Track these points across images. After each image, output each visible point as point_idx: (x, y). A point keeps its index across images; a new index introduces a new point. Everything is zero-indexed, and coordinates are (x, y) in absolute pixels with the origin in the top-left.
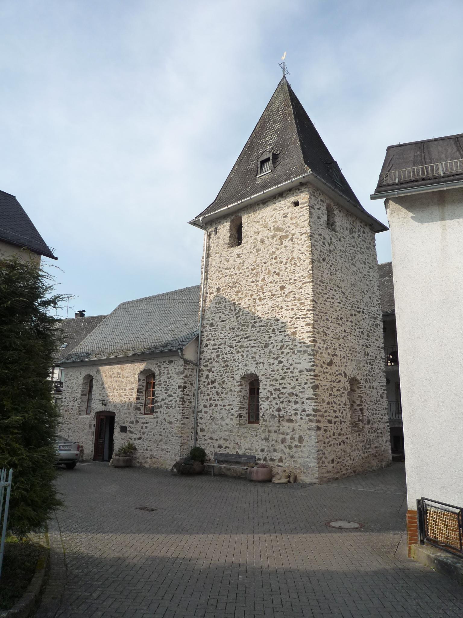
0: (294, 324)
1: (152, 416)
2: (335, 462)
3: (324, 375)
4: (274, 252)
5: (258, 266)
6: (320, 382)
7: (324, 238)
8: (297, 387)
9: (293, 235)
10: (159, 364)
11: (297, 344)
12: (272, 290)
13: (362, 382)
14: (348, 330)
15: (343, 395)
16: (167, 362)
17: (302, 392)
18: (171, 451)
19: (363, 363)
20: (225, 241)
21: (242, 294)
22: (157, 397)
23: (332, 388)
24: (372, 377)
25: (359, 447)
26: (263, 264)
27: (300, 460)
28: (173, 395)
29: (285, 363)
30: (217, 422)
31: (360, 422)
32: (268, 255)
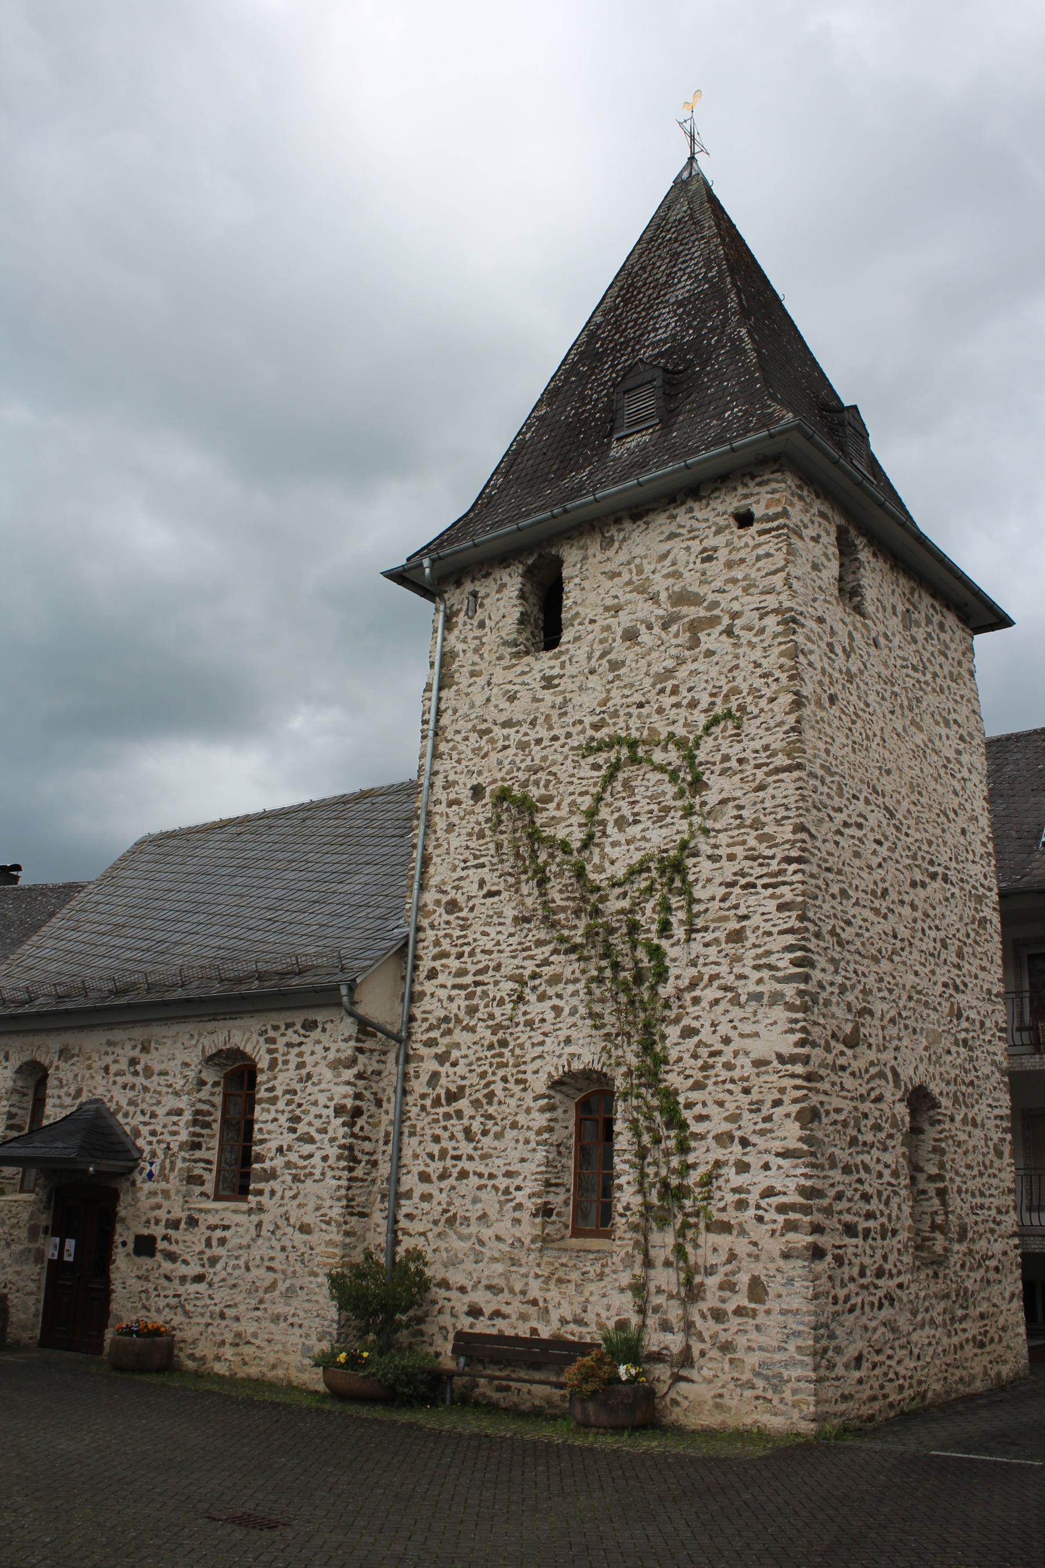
0: (736, 907)
1: (244, 1206)
2: (866, 1365)
3: (834, 1078)
4: (669, 673)
5: (615, 714)
6: (822, 1098)
7: (833, 633)
8: (746, 1115)
9: (735, 616)
10: (271, 1033)
11: (747, 971)
12: (664, 793)
13: (944, 1101)
14: (904, 933)
16: (298, 1027)
17: (762, 1133)
18: (306, 1323)
19: (947, 1042)
20: (503, 634)
21: (558, 807)
22: (262, 1141)
23: (857, 1120)
24: (970, 1090)
25: (935, 1315)
26: (633, 710)
27: (753, 1359)
28: (317, 1137)
29: (705, 1035)
30: (464, 1230)
32: (648, 682)
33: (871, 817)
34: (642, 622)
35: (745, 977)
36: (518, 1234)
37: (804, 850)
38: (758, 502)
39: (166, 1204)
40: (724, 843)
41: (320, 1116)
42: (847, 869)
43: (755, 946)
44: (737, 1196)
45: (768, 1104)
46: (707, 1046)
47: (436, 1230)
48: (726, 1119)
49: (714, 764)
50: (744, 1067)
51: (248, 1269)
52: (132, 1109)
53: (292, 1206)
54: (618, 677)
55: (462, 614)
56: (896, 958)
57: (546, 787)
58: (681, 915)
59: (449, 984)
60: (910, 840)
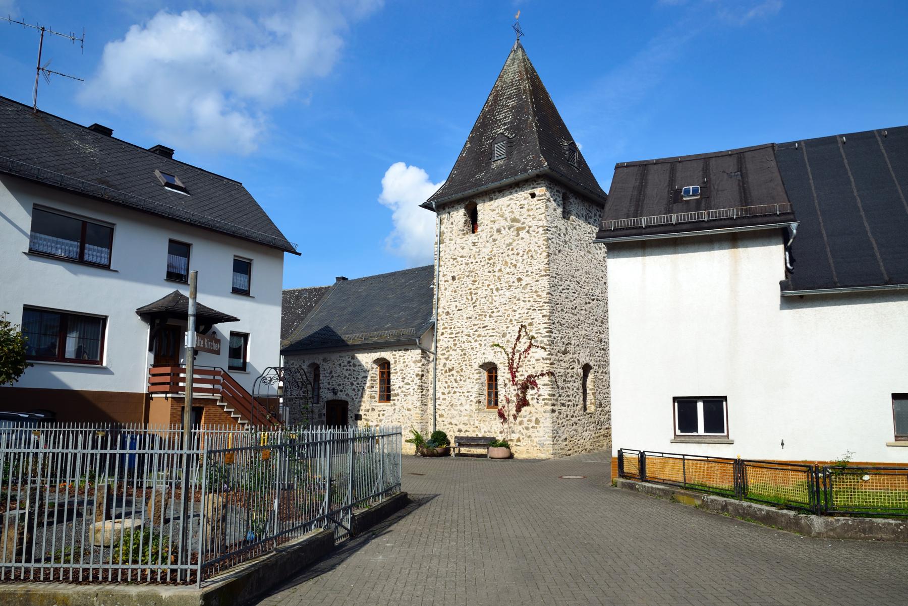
4: (510, 244)
14: (582, 318)
27: (536, 440)
53: (404, 404)
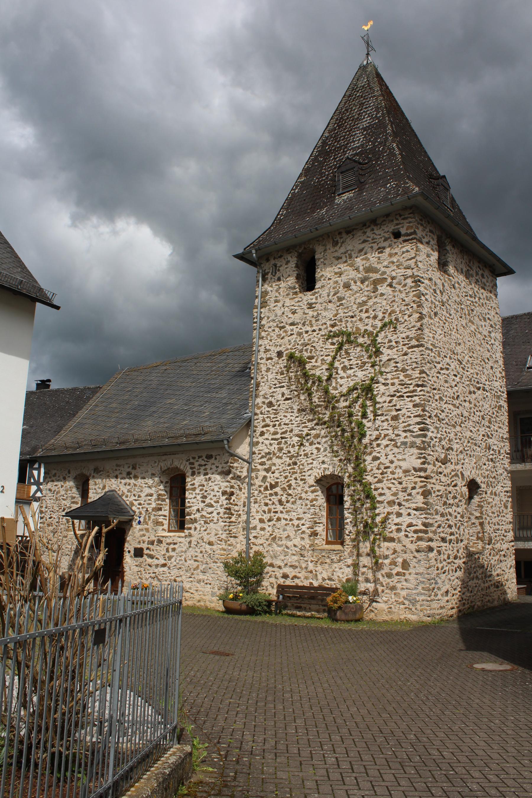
0: (395, 405)
1: (183, 534)
2: (450, 595)
3: (437, 477)
4: (364, 303)
6: (432, 486)
7: (436, 284)
9: (393, 278)
10: (192, 461)
11: (400, 433)
13: (483, 485)
14: (466, 414)
15: (460, 504)
16: (204, 457)
17: (407, 500)
18: (213, 583)
19: (484, 460)
21: (316, 362)
22: (190, 507)
23: (446, 494)
24: (494, 480)
27: (404, 593)
29: (383, 459)
30: (280, 543)
31: (479, 541)
32: (355, 306)
33: (452, 364)
34: (352, 279)
35: (400, 435)
36: (303, 544)
37: (424, 381)
38: (403, 227)
39: (147, 534)
40: (390, 378)
41: (216, 496)
42: (442, 388)
43: (403, 422)
44: (397, 527)
45: (409, 489)
46: (383, 464)
47: (267, 543)
48: (392, 495)
49: (385, 343)
50: (399, 473)
51: (186, 561)
52: (129, 494)
54: (342, 304)
55: (270, 274)
56: (462, 425)
57: (311, 352)
58: (371, 408)
59: (270, 438)
60: (468, 373)
